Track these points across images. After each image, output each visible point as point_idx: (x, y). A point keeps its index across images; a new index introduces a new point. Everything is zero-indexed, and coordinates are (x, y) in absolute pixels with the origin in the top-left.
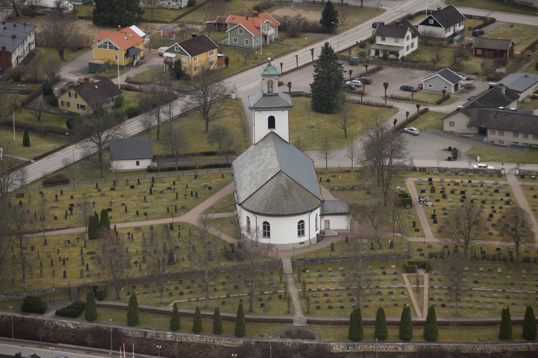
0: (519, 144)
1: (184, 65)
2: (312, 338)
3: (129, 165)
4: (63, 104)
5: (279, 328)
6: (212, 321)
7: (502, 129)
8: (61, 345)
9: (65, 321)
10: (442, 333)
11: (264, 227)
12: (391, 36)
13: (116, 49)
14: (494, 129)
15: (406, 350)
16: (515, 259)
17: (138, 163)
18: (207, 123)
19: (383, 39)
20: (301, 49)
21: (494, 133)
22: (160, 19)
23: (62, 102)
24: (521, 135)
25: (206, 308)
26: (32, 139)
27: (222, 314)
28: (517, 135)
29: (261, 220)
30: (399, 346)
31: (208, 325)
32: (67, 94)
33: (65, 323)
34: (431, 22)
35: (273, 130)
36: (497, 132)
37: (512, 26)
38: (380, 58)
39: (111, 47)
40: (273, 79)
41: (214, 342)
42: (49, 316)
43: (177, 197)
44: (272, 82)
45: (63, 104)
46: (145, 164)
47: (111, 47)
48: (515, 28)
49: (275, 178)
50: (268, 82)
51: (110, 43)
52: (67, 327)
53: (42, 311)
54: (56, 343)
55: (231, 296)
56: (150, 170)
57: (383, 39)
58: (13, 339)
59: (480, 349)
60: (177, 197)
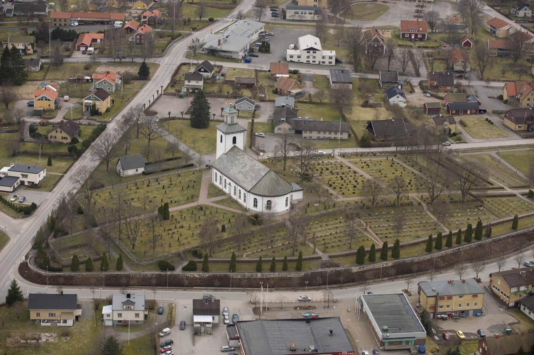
0: (321, 138)
1: (97, 107)
2: (338, 266)
3: (131, 172)
4: (51, 138)
5: (315, 262)
6: (282, 263)
7: (311, 131)
8: (196, 288)
9: (193, 273)
10: (402, 252)
11: (267, 204)
12: (195, 80)
13: (49, 100)
14: (306, 131)
15: (388, 265)
16: (397, 205)
17: (137, 170)
18: (149, 141)
19: (189, 82)
20: (140, 91)
21: (306, 132)
22: (33, 79)
23: (51, 136)
24: (322, 133)
25: (266, 256)
26: (53, 162)
27: (276, 259)
28: (320, 133)
29: (266, 199)
30: (385, 264)
31: (279, 266)
32: (55, 131)
33: (193, 275)
34: (203, 70)
35: (235, 145)
36: (308, 132)
37: (234, 69)
38: (190, 92)
39: (46, 99)
40: (234, 115)
41: (287, 276)
42: (178, 271)
43: (183, 189)
44: (234, 117)
45: (51, 138)
46: (141, 170)
47: (46, 99)
48: (236, 70)
49: (268, 175)
50: (232, 117)
51: (45, 97)
52: (194, 277)
53: (173, 269)
54: (193, 287)
55: (274, 247)
56: (144, 173)
57: (189, 82)
58: (168, 287)
59: (422, 259)
60: (183, 189)
